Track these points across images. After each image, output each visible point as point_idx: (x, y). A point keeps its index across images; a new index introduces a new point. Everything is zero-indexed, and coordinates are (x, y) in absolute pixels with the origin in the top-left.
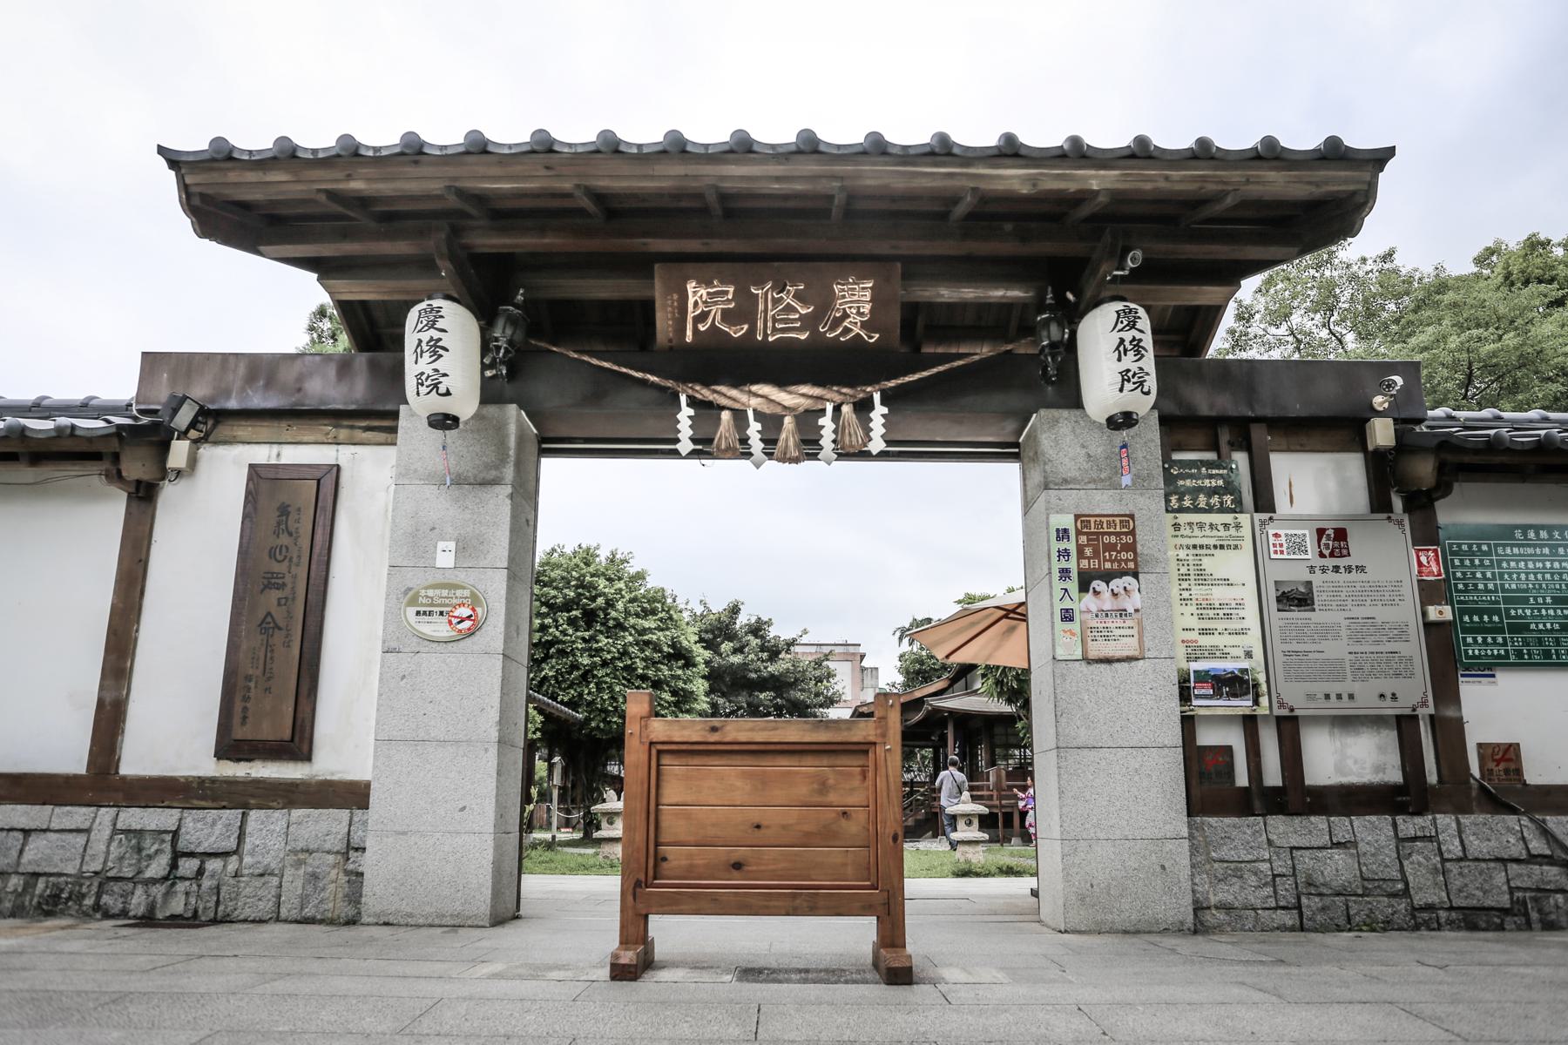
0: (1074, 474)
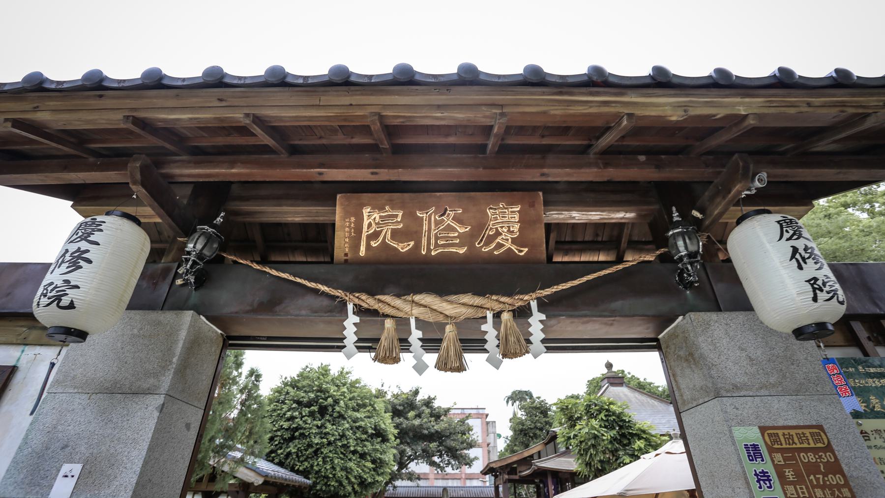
0: (740, 379)
